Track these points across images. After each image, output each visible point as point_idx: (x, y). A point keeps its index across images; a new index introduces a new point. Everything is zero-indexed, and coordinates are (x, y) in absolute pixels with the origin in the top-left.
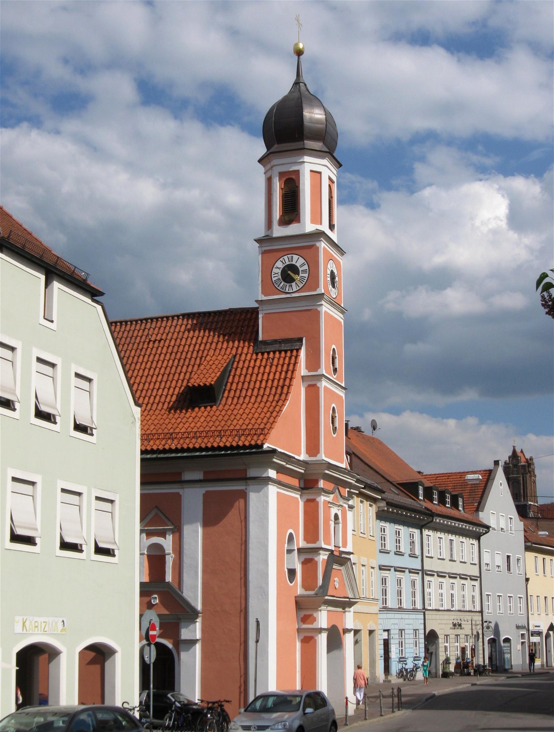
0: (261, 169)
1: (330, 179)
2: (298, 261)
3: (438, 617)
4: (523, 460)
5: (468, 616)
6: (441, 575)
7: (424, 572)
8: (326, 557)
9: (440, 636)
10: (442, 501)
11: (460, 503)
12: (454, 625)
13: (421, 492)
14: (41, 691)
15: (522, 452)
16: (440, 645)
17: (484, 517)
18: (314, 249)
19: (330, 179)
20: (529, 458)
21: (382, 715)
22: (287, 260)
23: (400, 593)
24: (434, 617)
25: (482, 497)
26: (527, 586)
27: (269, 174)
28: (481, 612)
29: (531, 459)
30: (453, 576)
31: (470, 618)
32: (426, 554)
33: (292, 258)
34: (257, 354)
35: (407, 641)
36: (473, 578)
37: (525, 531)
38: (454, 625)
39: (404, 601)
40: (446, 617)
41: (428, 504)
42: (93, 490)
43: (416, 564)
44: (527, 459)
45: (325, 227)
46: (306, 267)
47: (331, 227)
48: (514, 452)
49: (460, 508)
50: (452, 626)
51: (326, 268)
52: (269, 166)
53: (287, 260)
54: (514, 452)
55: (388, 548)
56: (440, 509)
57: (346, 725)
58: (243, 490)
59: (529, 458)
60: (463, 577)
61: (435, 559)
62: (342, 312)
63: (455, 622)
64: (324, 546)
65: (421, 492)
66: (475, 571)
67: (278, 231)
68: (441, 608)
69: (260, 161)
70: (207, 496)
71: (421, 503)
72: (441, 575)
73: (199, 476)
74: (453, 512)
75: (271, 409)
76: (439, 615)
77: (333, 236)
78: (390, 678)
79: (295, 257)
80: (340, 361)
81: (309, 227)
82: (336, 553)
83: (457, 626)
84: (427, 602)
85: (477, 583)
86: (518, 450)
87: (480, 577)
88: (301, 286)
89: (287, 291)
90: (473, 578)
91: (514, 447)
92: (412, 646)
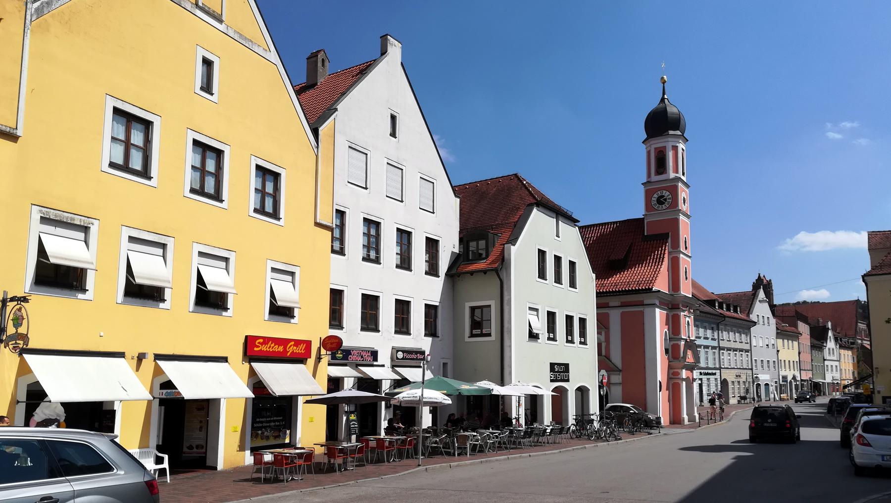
0: (644, 146)
1: (683, 149)
2: (666, 194)
3: (727, 372)
4: (765, 281)
5: (745, 371)
6: (729, 349)
7: (721, 348)
8: (684, 343)
9: (729, 382)
10: (728, 309)
11: (739, 310)
12: (737, 376)
13: (717, 305)
14: (503, 410)
15: (764, 276)
16: (729, 387)
17: (753, 317)
18: (676, 187)
19: (683, 149)
20: (768, 280)
21: (708, 424)
22: (660, 193)
23: (707, 359)
24: (725, 372)
25: (751, 306)
26: (778, 354)
27: (649, 149)
28: (752, 369)
29: (770, 280)
30: (735, 350)
31: (745, 372)
32: (721, 338)
33: (669, 195)
34: (644, 242)
35: (711, 384)
36: (747, 351)
37: (776, 324)
38: (737, 376)
39: (709, 363)
40: (732, 372)
41: (720, 311)
42: (546, 307)
43: (715, 344)
44: (767, 281)
45: (680, 175)
46: (670, 196)
47: (683, 174)
48: (759, 276)
49: (739, 313)
50: (735, 377)
51: (681, 195)
52: (649, 144)
53: (660, 193)
54: (759, 276)
55: (700, 335)
56: (728, 313)
57: (700, 427)
58: (641, 311)
59: (768, 280)
60: (741, 350)
61: (744, 343)
62: (688, 218)
63: (737, 374)
64: (683, 337)
65: (717, 305)
66: (747, 347)
67: (655, 178)
68: (742, 367)
69: (643, 143)
70: (623, 314)
71: (718, 310)
72: (729, 349)
73: (617, 304)
74: (735, 315)
75: (655, 270)
76: (727, 371)
77: (684, 178)
78: (703, 404)
79: (664, 192)
80: (689, 244)
81: (672, 175)
82: (688, 340)
83: (738, 376)
84: (722, 363)
85: (749, 354)
86: (762, 276)
87: (751, 350)
88: (668, 206)
89: (660, 209)
90: (747, 351)
91: (759, 274)
92: (714, 387)
